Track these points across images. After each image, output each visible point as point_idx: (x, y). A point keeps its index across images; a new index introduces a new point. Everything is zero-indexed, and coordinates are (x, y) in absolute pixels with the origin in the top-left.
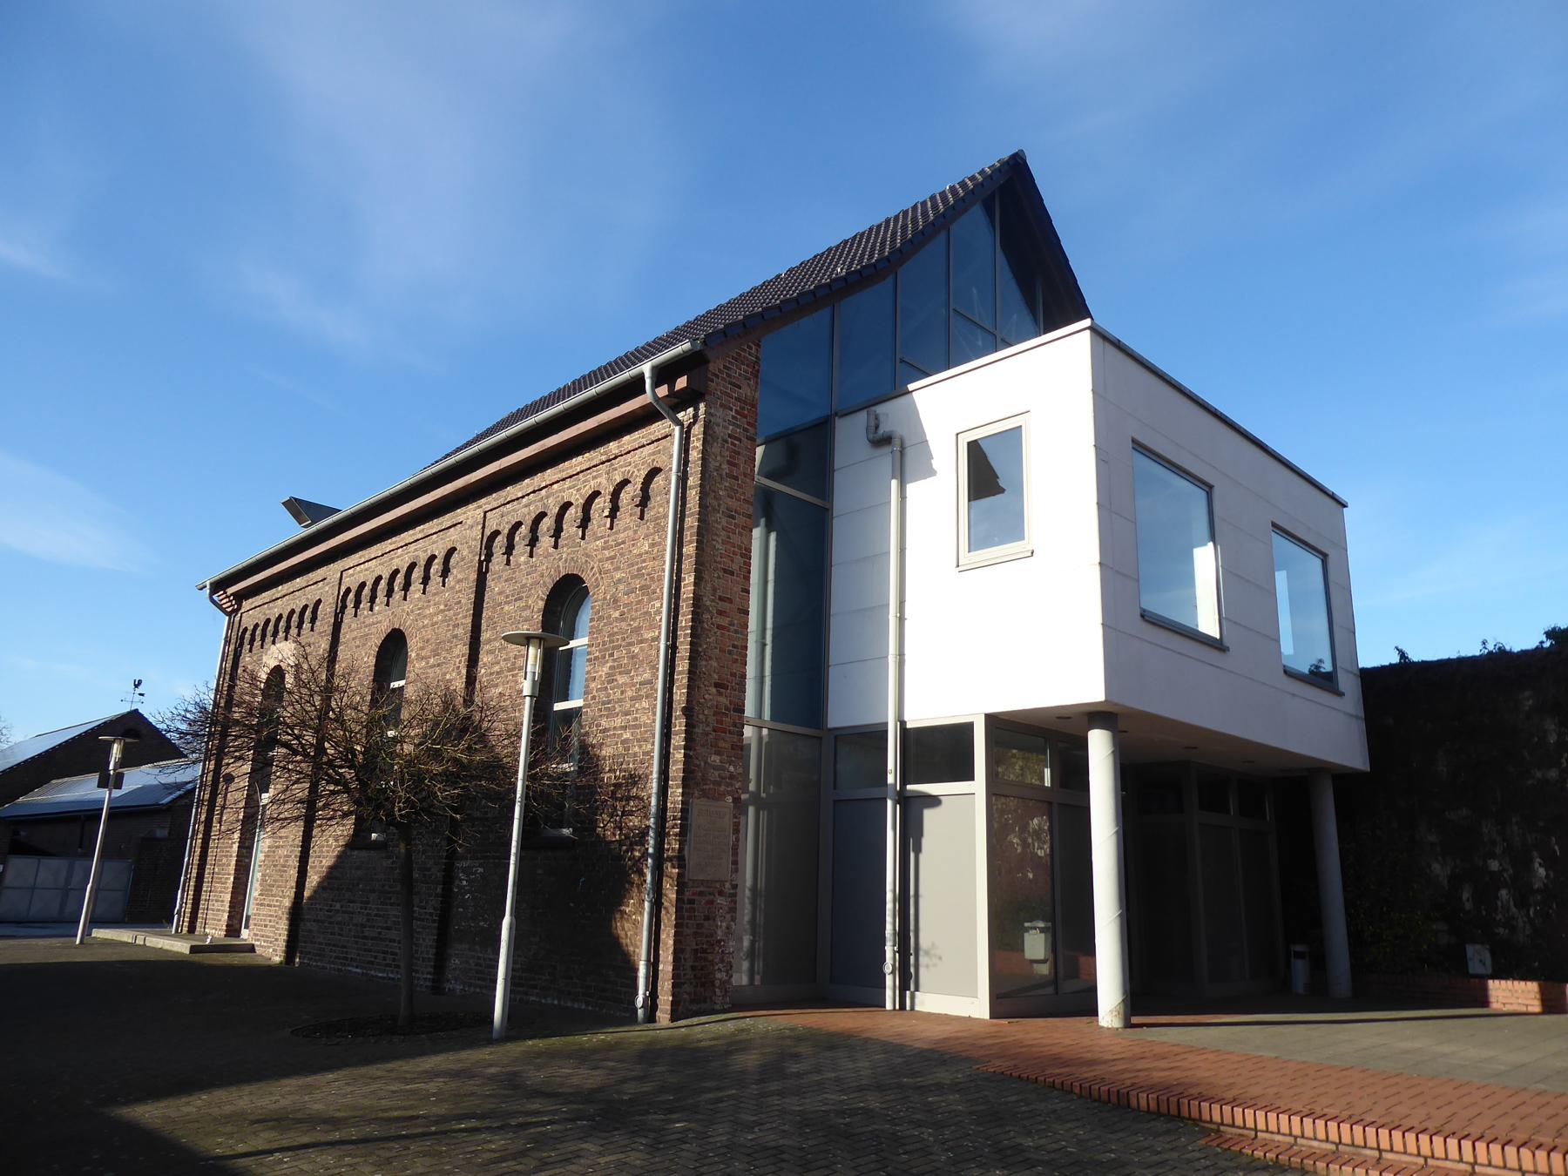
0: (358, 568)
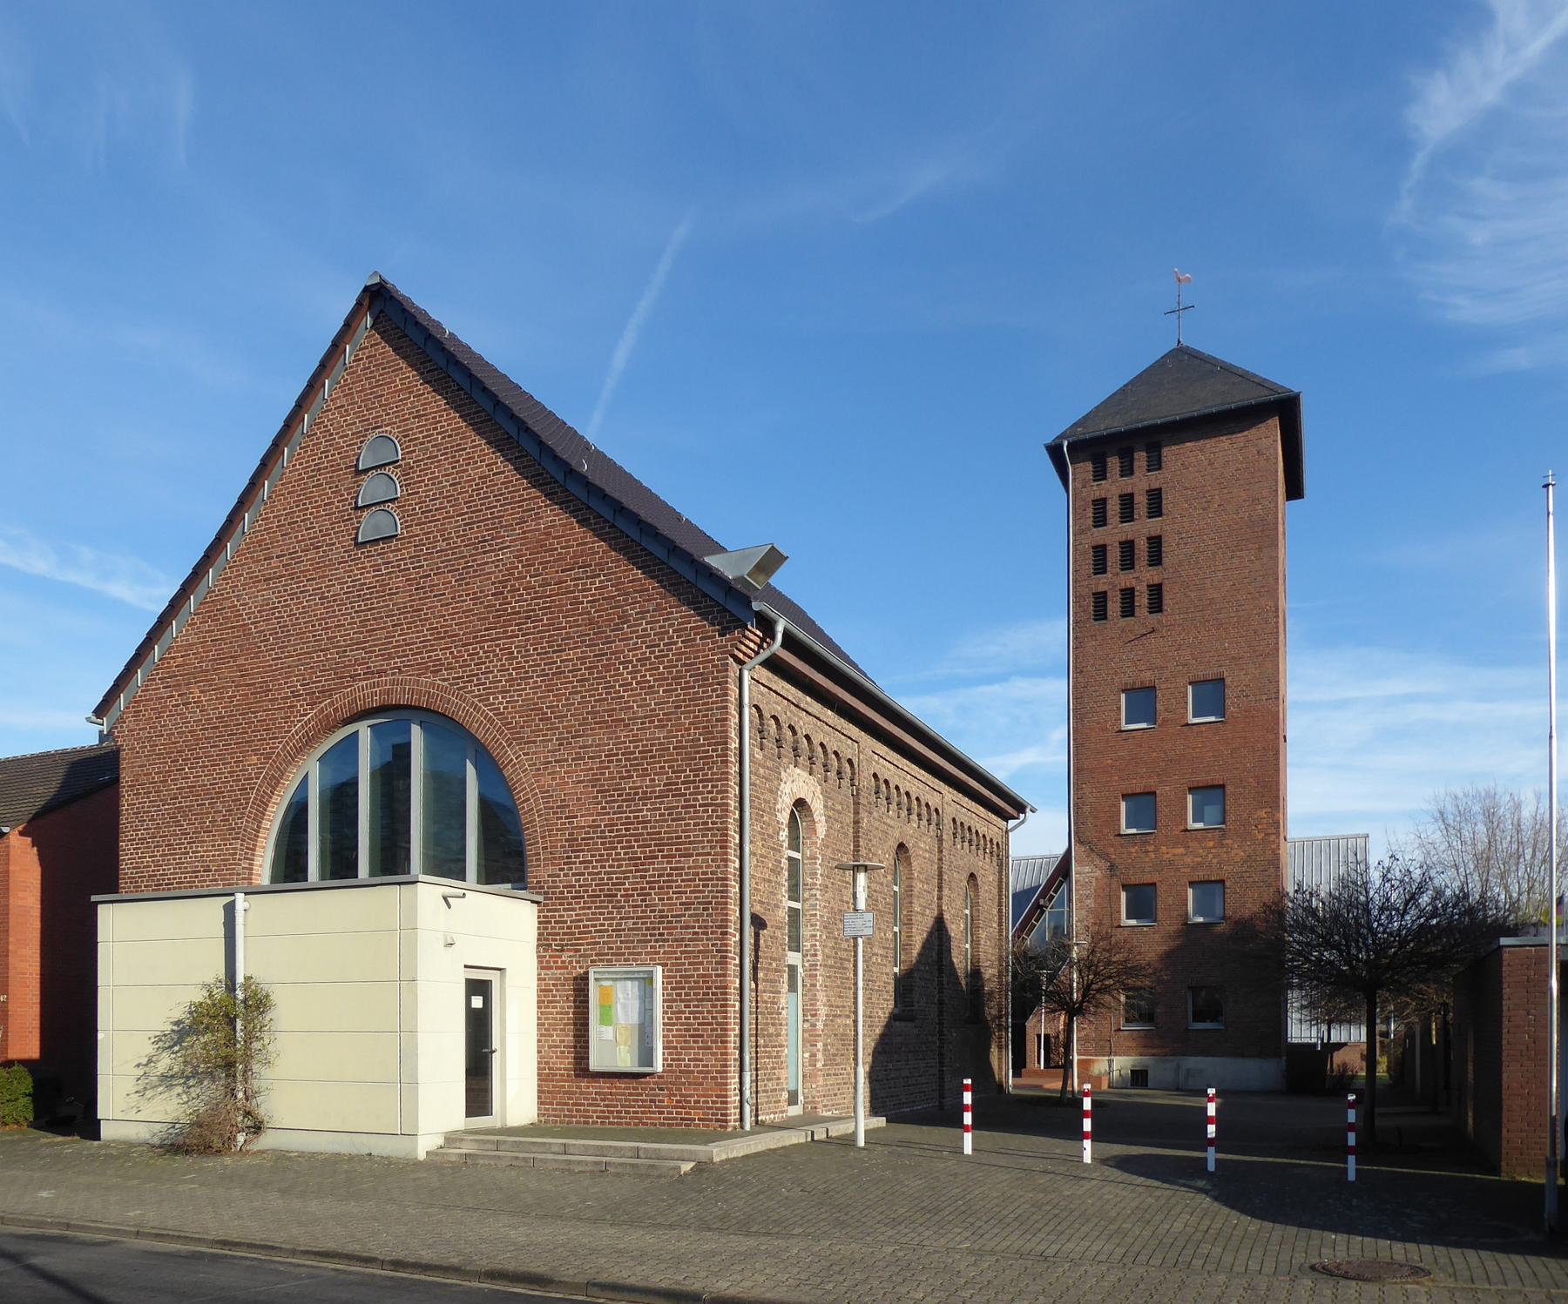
0: (881, 760)
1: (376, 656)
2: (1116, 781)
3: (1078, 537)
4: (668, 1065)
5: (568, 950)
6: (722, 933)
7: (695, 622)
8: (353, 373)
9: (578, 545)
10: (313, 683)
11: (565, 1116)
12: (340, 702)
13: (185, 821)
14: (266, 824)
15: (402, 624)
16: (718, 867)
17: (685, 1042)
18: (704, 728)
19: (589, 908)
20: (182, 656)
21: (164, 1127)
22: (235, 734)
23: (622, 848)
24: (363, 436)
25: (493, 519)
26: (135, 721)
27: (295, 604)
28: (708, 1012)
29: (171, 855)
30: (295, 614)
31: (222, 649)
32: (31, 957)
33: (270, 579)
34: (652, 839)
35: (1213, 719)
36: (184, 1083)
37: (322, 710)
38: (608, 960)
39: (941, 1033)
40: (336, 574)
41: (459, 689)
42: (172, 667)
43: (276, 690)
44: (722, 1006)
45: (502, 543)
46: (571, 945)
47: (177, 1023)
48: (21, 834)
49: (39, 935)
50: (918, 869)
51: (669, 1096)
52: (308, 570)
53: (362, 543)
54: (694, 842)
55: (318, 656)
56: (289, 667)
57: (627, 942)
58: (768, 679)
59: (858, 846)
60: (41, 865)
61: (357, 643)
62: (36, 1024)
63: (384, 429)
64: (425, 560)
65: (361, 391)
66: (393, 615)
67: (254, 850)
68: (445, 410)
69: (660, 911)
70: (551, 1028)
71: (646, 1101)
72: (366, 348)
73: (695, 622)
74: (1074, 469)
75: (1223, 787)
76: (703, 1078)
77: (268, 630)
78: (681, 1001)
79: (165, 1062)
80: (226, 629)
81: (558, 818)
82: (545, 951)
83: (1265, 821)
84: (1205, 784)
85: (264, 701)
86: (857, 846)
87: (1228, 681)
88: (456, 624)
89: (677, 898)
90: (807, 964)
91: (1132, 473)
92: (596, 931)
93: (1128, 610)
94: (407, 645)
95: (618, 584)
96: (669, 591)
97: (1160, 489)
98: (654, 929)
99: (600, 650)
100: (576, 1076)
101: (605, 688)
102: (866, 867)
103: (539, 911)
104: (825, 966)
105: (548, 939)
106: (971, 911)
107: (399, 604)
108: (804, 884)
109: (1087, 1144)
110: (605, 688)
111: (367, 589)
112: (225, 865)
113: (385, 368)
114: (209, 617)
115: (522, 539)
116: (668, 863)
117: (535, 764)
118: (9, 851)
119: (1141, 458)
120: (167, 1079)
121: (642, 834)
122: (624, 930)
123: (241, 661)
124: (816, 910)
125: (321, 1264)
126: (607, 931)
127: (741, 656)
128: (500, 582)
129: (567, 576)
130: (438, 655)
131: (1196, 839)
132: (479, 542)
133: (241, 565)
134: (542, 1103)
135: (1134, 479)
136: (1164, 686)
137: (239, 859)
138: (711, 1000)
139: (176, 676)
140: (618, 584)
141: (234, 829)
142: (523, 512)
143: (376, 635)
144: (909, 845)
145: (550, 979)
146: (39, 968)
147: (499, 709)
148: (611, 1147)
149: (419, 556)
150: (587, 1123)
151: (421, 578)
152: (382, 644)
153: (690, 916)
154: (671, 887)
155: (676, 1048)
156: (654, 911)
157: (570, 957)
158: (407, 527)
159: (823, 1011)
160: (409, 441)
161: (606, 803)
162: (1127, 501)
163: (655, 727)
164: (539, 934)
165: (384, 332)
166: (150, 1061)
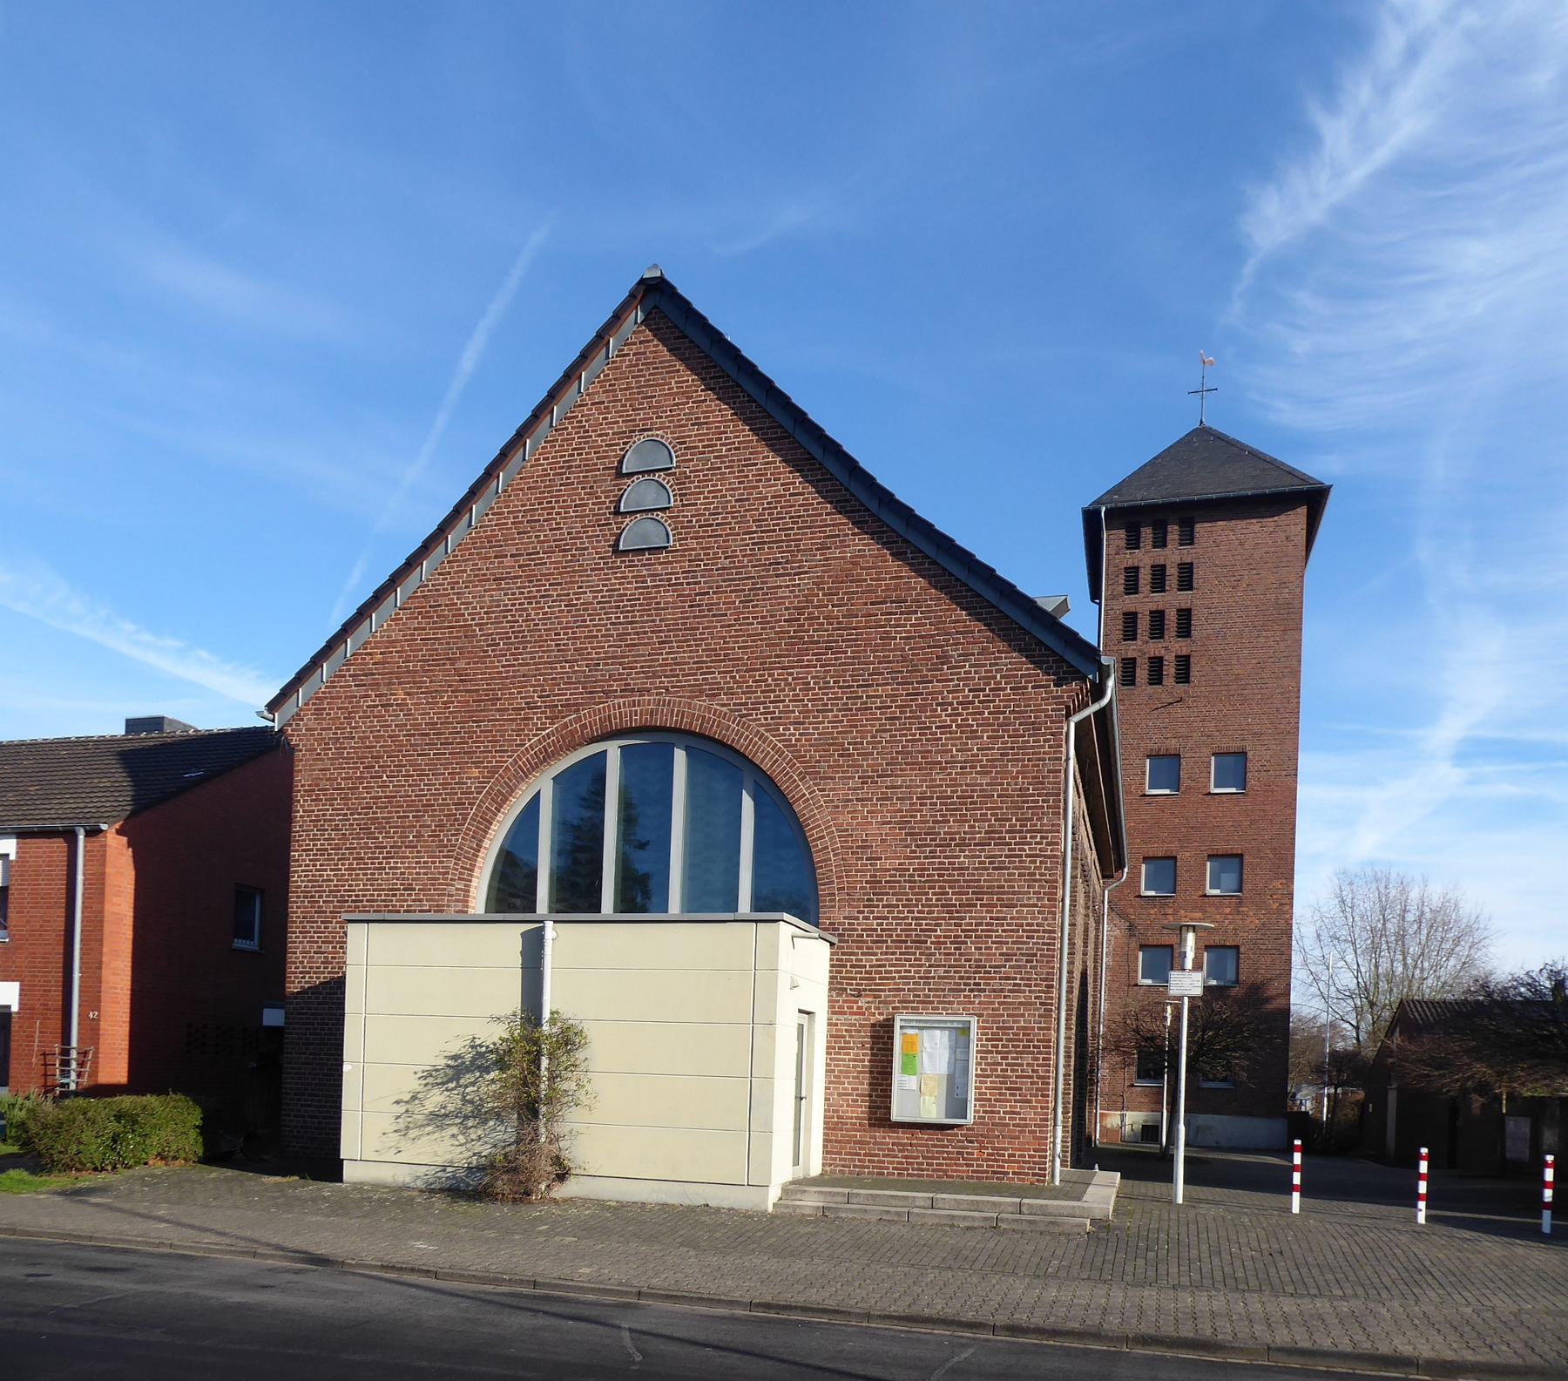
1: (636, 673)
2: (1138, 844)
3: (1109, 602)
4: (979, 1118)
5: (867, 996)
6: (1047, 986)
7: (1027, 669)
8: (617, 368)
9: (891, 579)
10: (555, 695)
11: (855, 1166)
12: (591, 717)
13: (380, 833)
14: (486, 843)
15: (672, 642)
16: (1046, 919)
17: (1000, 1094)
18: (1033, 777)
19: (893, 953)
20: (381, 653)
21: (432, 1171)
22: (452, 743)
23: (934, 894)
24: (627, 437)
25: (788, 541)
26: (315, 719)
27: (533, 609)
28: (1028, 1065)
29: (360, 869)
30: (533, 620)
31: (437, 650)
32: (123, 970)
33: (502, 579)
34: (968, 887)
35: (1233, 790)
36: (461, 1123)
37: (565, 726)
38: (913, 1008)
40: (588, 581)
41: (741, 716)
42: (368, 664)
43: (506, 699)
44: (1044, 1059)
45: (799, 567)
46: (870, 990)
47: (455, 1058)
48: (119, 832)
49: (131, 946)
51: (980, 1148)
52: (553, 574)
53: (622, 551)
54: (1019, 893)
55: (564, 667)
56: (524, 676)
57: (937, 990)
60: (135, 868)
61: (613, 658)
62: (125, 1044)
63: (654, 432)
64: (702, 577)
65: (625, 389)
66: (660, 631)
67: (472, 870)
68: (732, 421)
69: (976, 960)
70: (842, 1075)
71: (952, 1153)
72: (634, 344)
73: (1027, 669)
74: (1108, 536)
75: (1241, 856)
76: (1020, 1132)
77: (497, 634)
78: (997, 1052)
79: (436, 1099)
80: (440, 628)
81: (857, 859)
82: (838, 995)
83: (1280, 892)
84: (1225, 853)
85: (491, 710)
87: (1250, 754)
88: (739, 648)
89: (996, 949)
91: (1164, 545)
92: (900, 978)
93: (1156, 678)
94: (676, 664)
95: (939, 623)
96: (999, 636)
97: (1191, 564)
98: (969, 978)
99: (914, 688)
100: (870, 1125)
101: (919, 729)
102: (1194, 927)
105: (842, 984)
107: (668, 619)
109: (1296, 1196)
110: (919, 729)
111: (628, 600)
112: (434, 885)
113: (657, 368)
114: (420, 613)
115: (824, 565)
116: (987, 912)
117: (832, 801)
118: (105, 851)
119: (1173, 532)
120: (438, 1119)
121: (959, 881)
122: (934, 978)
123: (461, 664)
125: (936, 1332)
126: (914, 978)
128: (795, 608)
129: (878, 609)
130: (716, 678)
131: (1213, 905)
132: (770, 564)
133: (464, 561)
134: (828, 1153)
135: (1168, 551)
136: (1188, 755)
137: (451, 879)
138: (1033, 1053)
139: (373, 674)
140: (939, 623)
141: (446, 846)
142: (825, 537)
143: (639, 650)
145: (842, 1024)
146: (129, 983)
147: (791, 740)
148: (988, 1202)
149: (695, 571)
151: (696, 595)
152: (645, 661)
153: (1011, 967)
154: (991, 937)
155: (990, 1100)
156: (970, 960)
157: (868, 1002)
158: (680, 539)
160: (685, 449)
161: (917, 846)
162: (1159, 572)
163: (977, 773)
164: (831, 978)
165: (658, 329)
166: (414, 1098)
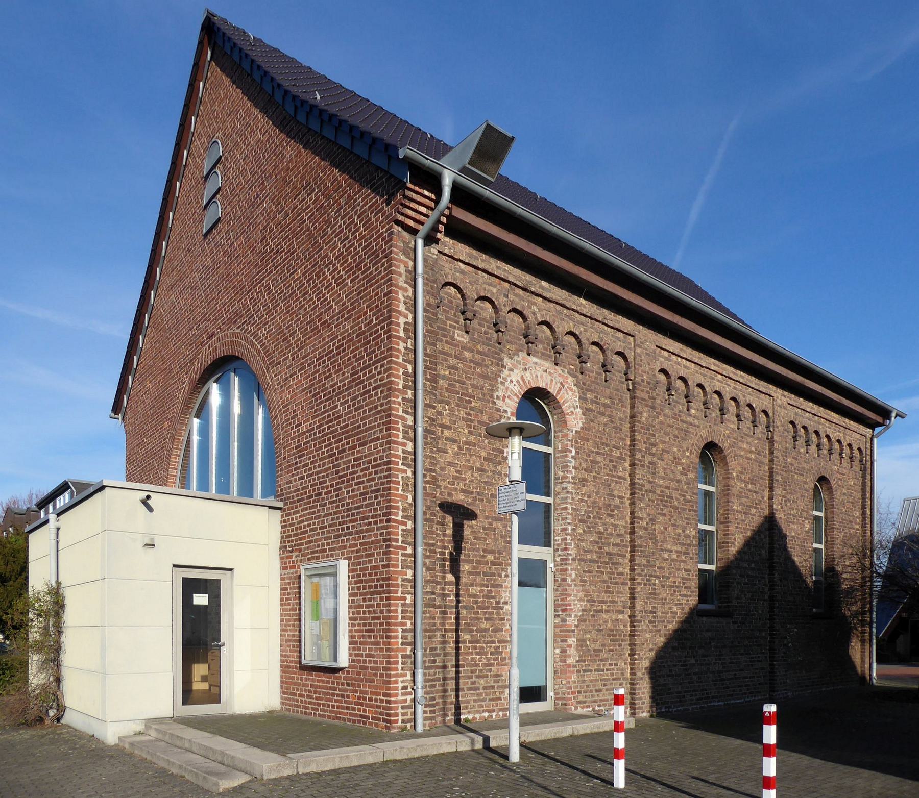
0: (674, 357)
4: (353, 661)
39: (772, 628)
50: (739, 469)
58: (471, 256)
59: (634, 440)
86: (633, 440)
90: (557, 559)
103: (282, 516)
104: (581, 560)
106: (826, 513)
108: (556, 479)
124: (567, 503)
127: (411, 223)
144: (725, 445)
150: (306, 713)
159: (577, 607)
